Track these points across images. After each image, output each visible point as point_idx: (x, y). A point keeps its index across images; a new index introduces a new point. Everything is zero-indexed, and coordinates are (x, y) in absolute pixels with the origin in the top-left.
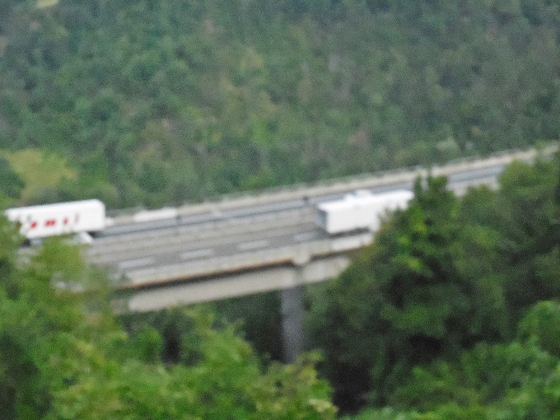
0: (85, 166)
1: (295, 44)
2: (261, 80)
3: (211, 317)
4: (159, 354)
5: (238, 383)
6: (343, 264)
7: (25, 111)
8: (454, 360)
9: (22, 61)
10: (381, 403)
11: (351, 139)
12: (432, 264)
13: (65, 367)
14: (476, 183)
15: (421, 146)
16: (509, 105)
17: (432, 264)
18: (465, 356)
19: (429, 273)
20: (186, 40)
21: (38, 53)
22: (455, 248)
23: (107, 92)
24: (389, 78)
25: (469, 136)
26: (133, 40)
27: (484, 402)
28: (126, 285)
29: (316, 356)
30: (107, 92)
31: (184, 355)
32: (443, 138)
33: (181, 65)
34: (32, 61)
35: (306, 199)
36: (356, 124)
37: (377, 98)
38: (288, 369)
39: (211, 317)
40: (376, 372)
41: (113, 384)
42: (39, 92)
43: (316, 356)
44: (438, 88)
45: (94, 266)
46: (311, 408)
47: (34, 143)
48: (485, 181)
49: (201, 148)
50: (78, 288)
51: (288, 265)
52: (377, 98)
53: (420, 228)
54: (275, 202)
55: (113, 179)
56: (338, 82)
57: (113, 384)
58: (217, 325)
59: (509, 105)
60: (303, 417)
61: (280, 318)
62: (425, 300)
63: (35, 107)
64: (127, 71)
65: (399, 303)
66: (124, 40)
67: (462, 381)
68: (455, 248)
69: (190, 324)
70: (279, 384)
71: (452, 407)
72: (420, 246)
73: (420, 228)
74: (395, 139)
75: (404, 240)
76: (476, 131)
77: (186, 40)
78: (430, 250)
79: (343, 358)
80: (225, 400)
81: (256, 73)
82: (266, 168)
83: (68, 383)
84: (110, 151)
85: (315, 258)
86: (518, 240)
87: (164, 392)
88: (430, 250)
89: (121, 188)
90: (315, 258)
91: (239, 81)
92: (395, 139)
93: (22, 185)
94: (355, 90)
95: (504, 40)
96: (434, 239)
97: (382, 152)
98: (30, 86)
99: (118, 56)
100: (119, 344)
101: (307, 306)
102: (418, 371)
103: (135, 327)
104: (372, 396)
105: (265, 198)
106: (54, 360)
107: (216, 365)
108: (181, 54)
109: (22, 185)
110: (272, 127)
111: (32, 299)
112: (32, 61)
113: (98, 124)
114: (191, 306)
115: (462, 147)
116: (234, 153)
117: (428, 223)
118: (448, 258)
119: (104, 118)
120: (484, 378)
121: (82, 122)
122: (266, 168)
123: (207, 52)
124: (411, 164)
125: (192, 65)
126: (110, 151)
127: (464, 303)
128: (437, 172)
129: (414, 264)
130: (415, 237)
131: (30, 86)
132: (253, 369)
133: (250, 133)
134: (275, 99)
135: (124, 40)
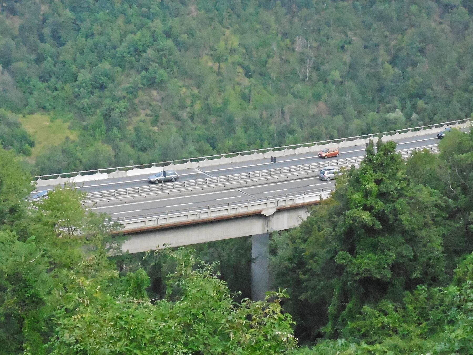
0: (85, 129)
1: (267, 28)
2: (236, 58)
3: (193, 260)
4: (295, 225)
5: (215, 316)
6: (304, 215)
7: (35, 81)
8: (397, 299)
9: (34, 38)
10: (335, 336)
11: (313, 110)
12: (380, 216)
13: (69, 299)
14: (420, 148)
15: (373, 116)
16: (449, 82)
17: (380, 216)
18: (408, 296)
19: (378, 226)
20: (174, 23)
21: (47, 31)
22: (400, 204)
23: (106, 66)
24: (347, 58)
25: (414, 107)
26: (128, 22)
27: (422, 336)
28: (120, 230)
29: (281, 294)
30: (106, 66)
31: (169, 291)
32: (393, 110)
33: (169, 43)
34: (42, 39)
35: (273, 159)
36: (317, 97)
37: (336, 75)
38: (258, 304)
39: (193, 260)
40: (331, 309)
41: (108, 315)
42: (48, 64)
43: (281, 294)
44: (388, 66)
45: (92, 214)
46: (275, 338)
47: (42, 108)
48: (428, 147)
49: (184, 115)
50: (78, 233)
51: (258, 215)
52: (336, 75)
53: (372, 186)
54: (247, 162)
55: (109, 141)
56: (302, 61)
57: (108, 315)
58: (196, 267)
59: (449, 82)
60: (420, 277)
61: (250, 261)
62: (374, 247)
63: (44, 79)
64: (122, 49)
65: (352, 251)
66: (121, 21)
67: (405, 318)
68: (400, 204)
69: (174, 266)
70: (249, 317)
71: (396, 340)
72: (371, 201)
73: (372, 186)
74: (351, 110)
75: (357, 196)
76: (421, 103)
77: (174, 23)
78: (380, 205)
79: (302, 297)
80: (202, 329)
81: (232, 51)
82: (239, 132)
83: (69, 313)
84: (106, 116)
85: (280, 211)
86: (455, 199)
87: (151, 322)
88: (380, 205)
89: (116, 148)
90: (280, 211)
91: (218, 59)
92: (351, 110)
93: (32, 144)
94: (316, 68)
95: (446, 26)
96: (381, 195)
97: (339, 120)
98: (40, 60)
99: (115, 35)
100: (112, 280)
101: (273, 252)
102: (367, 308)
103: (127, 267)
104: (327, 329)
105: (238, 159)
106: (57, 293)
107: (196, 300)
108: (168, 35)
109: (32, 144)
110: (246, 98)
111: (38, 240)
112: (42, 39)
113: (97, 93)
114: (176, 249)
115: (408, 117)
116: (212, 120)
117: (378, 182)
118: (395, 212)
119: (102, 87)
120: (423, 315)
121: (83, 91)
122: (239, 132)
123: (190, 33)
124: (364, 133)
125: (177, 44)
126: (106, 116)
127: (408, 251)
128: (386, 139)
129: (366, 217)
130: (367, 194)
131: (40, 60)
132: (227, 303)
133: (226, 103)
134: (248, 75)
135: (121, 21)
